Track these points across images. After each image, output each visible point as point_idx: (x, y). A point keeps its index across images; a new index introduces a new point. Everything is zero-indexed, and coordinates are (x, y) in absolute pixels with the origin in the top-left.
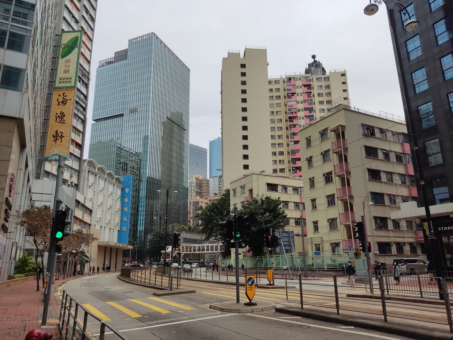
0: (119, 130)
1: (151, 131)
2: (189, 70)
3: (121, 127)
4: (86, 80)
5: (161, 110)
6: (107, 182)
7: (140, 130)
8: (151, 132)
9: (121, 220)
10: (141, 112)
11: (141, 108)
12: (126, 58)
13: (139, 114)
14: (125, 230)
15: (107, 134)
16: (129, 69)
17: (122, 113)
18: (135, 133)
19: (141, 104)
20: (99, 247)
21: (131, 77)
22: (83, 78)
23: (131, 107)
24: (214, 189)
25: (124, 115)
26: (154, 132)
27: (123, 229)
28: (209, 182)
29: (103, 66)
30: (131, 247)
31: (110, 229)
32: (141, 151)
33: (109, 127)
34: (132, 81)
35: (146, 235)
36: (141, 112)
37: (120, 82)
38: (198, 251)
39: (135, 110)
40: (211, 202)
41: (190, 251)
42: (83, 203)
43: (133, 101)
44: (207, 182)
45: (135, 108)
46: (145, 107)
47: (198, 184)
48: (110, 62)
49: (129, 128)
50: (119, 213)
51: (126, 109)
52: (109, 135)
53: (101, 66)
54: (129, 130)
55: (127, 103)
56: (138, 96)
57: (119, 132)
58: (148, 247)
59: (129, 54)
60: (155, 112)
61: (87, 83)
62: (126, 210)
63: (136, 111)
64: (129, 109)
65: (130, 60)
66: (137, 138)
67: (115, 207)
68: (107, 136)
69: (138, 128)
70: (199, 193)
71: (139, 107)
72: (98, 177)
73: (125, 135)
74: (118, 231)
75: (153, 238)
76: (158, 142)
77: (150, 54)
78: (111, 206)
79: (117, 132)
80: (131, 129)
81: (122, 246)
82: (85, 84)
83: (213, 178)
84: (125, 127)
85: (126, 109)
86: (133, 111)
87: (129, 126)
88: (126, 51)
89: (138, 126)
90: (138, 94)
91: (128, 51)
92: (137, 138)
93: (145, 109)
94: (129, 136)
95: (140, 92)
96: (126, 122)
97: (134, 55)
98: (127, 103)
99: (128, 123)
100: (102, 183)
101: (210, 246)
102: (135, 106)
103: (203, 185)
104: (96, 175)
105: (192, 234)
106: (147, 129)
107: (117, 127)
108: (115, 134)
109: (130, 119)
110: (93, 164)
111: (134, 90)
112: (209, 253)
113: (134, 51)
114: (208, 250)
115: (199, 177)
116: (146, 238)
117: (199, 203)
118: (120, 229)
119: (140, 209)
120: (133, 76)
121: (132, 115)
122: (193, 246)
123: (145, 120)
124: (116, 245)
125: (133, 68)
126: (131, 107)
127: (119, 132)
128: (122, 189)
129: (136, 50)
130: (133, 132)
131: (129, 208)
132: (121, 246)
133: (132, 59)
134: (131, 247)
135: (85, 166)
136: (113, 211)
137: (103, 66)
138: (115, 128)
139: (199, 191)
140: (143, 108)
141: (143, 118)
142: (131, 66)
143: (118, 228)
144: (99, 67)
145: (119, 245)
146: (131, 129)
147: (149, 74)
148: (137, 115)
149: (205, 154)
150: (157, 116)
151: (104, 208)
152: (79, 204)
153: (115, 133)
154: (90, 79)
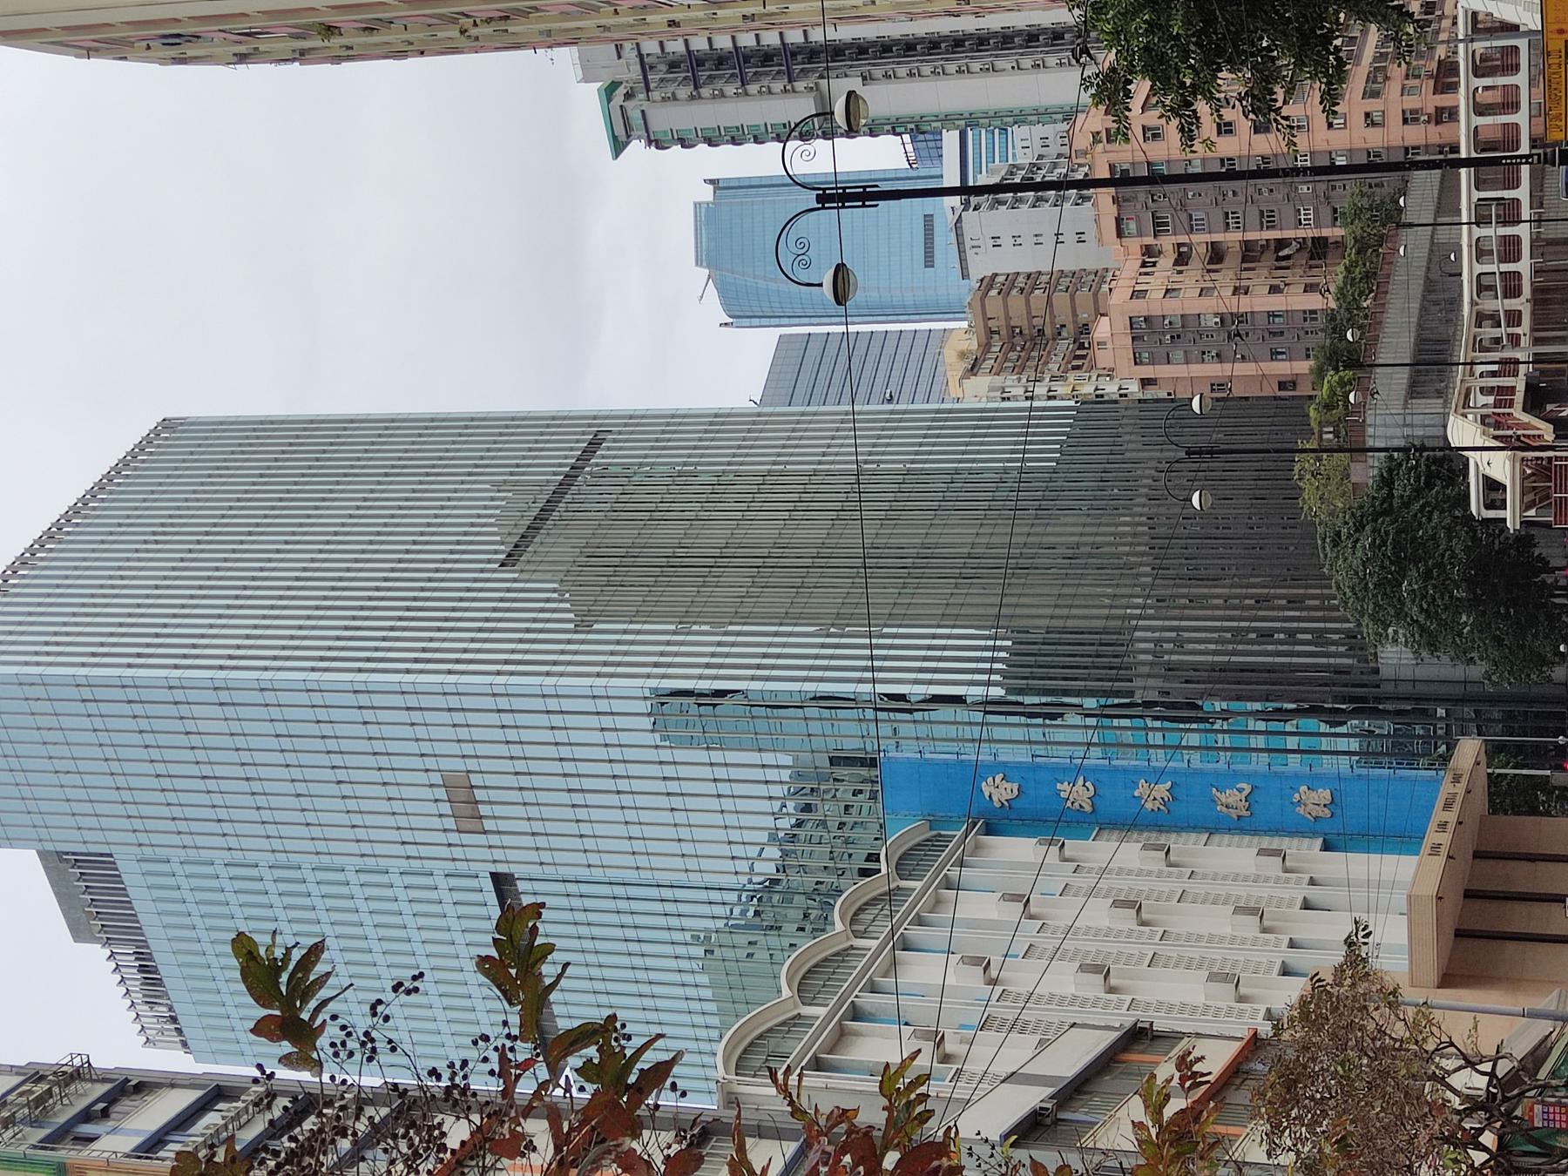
0: (610, 904)
1: (598, 675)
2: (168, 424)
3: (585, 888)
4: (85, 1095)
5: (454, 609)
6: (916, 933)
7: (601, 753)
8: (612, 675)
9: (1240, 826)
10: (468, 749)
11: (440, 748)
12: (105, 862)
13: (486, 765)
14: (1324, 795)
15: (645, 989)
16: (175, 839)
17: (488, 885)
18: (623, 785)
19: (413, 747)
20: (1448, 980)
21: (227, 828)
22: (62, 1119)
23: (436, 823)
25: (501, 868)
26: (612, 653)
28: (1001, 279)
29: (174, 1020)
30: (1469, 750)
31: (1307, 906)
33: (595, 972)
34: (254, 816)
36: (468, 749)
37: (375, 945)
38: (1516, 258)
39: (462, 794)
40: (1133, 226)
41: (1514, 318)
42: (1050, 1091)
43: (397, 806)
44: (994, 292)
45: (441, 793)
46: (430, 717)
47: (1014, 356)
48: (142, 969)
49: (585, 829)
50: (1186, 845)
51: (458, 852)
52: (653, 976)
53: (179, 1031)
54: (600, 829)
55: (412, 851)
56: (355, 775)
57: (623, 905)
58: (1477, 671)
59: (71, 842)
60: (465, 651)
61: (102, 1089)
62: (1162, 790)
64: (454, 838)
65: (112, 836)
66: (656, 770)
67: (1130, 872)
68: (657, 990)
69: (584, 768)
70: (1081, 347)
71: (430, 763)
72: (868, 1001)
73: (642, 861)
74: (1327, 847)
75: (1400, 615)
77: (55, 692)
79: (627, 919)
80: (596, 814)
81: (1457, 807)
82: (112, 1098)
83: (970, 253)
84: (580, 858)
85: (458, 852)
86: (466, 809)
87: (573, 828)
88: (58, 864)
89: (569, 767)
90: (341, 774)
91: (49, 847)
92: (656, 770)
93: (445, 717)
94: (649, 831)
95: (324, 760)
96: (546, 856)
97: (77, 808)
98: (412, 851)
99: (556, 842)
100: (921, 971)
101: (1476, 195)
102: (427, 793)
104: (856, 1014)
105: (1376, 338)
106: (588, 705)
107: (592, 917)
108: (643, 934)
109: (524, 826)
110: (760, 1037)
111: (320, 803)
112: (1537, 200)
113: (44, 806)
114: (1510, 250)
115: (963, 355)
117: (1146, 319)
118: (1313, 834)
120: (222, 813)
121: (499, 810)
122: (1473, 303)
123: (522, 719)
124: (1444, 851)
125: (165, 811)
126: (436, 823)
127: (623, 905)
128: (990, 830)
129: (39, 792)
130: (613, 800)
131: (1138, 772)
133: (105, 823)
134: (1469, 750)
136: (1164, 886)
137: (174, 1020)
138: (596, 931)
139: (1064, 346)
140: (436, 733)
141: (512, 735)
142: (150, 824)
143: (1307, 851)
144: (184, 1044)
145: (1436, 848)
146: (596, 814)
147: (193, 695)
148: (491, 780)
149: (814, 349)
151: (1134, 949)
152: (1057, 1121)
153: (631, 933)
154: (77, 1062)
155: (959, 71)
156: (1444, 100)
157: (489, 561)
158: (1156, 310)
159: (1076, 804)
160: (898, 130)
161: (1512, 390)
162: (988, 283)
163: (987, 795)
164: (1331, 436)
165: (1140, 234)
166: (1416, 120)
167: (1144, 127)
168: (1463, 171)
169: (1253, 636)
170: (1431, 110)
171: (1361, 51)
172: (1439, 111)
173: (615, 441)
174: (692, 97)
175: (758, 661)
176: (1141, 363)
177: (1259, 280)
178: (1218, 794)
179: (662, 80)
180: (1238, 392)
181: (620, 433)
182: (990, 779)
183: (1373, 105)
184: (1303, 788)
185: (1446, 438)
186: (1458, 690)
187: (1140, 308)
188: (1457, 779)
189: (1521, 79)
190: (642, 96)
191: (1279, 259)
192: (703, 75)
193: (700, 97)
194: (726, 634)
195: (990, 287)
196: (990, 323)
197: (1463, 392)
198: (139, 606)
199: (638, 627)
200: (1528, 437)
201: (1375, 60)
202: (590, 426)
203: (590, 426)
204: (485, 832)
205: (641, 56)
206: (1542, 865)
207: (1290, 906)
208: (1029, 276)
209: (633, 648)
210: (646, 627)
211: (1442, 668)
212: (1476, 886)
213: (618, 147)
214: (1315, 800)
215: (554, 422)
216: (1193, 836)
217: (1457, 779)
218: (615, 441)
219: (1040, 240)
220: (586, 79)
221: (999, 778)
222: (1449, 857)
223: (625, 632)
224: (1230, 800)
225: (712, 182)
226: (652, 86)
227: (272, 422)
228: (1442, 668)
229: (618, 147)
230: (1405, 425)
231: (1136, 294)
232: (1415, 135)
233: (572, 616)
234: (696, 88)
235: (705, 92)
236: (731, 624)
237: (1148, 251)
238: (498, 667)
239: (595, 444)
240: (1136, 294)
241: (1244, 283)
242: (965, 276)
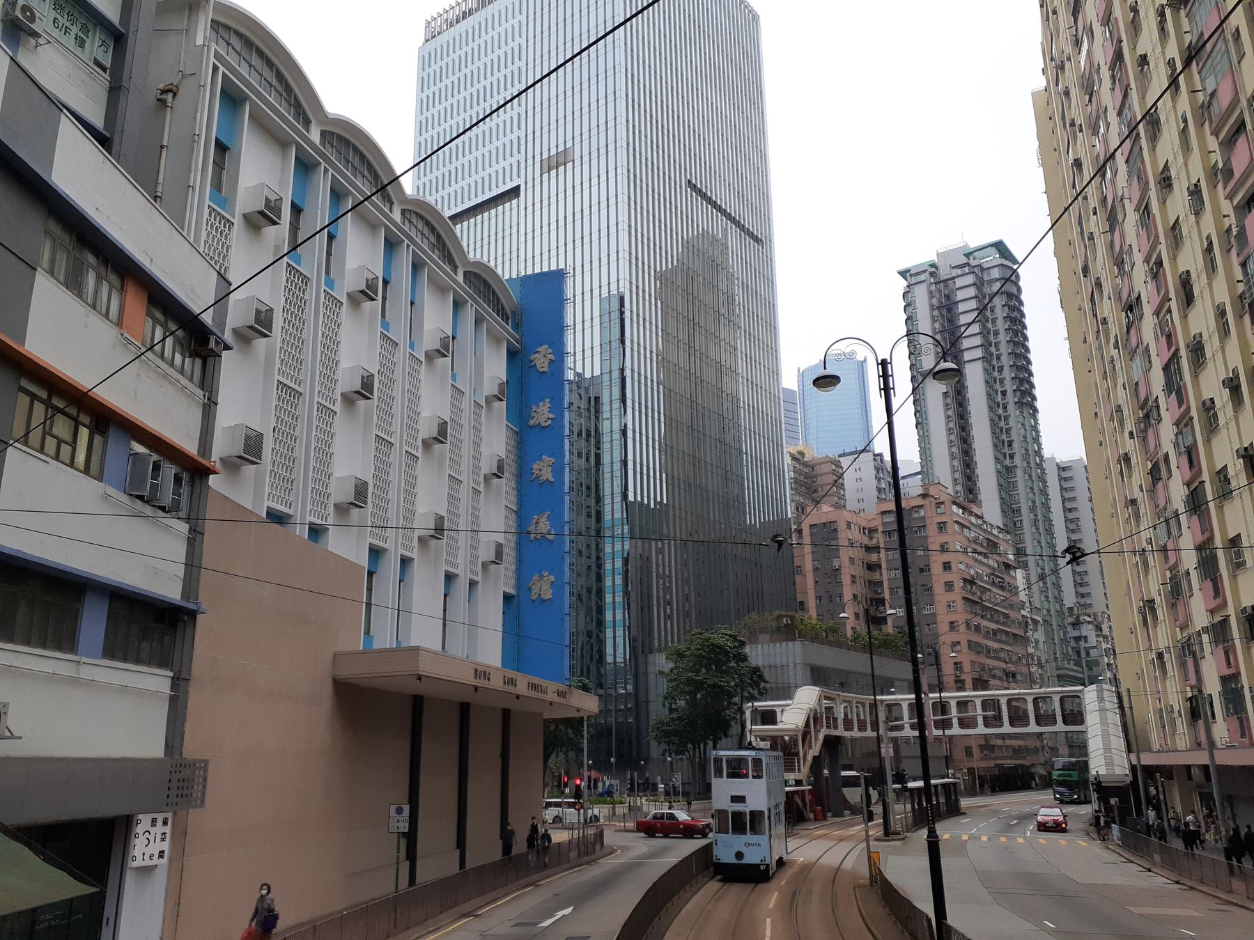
2: (755, 18)
9: (522, 533)
14: (548, 595)
24: (860, 496)
27: (535, 590)
31: (450, 578)
32: (597, 373)
35: (641, 658)
39: (561, 160)
44: (834, 467)
48: (464, 13)
50: (505, 485)
60: (641, 180)
62: (547, 474)
63: (567, 160)
74: (508, 598)
76: (640, 404)
78: (440, 519)
81: (533, 694)
86: (554, 163)
103: (818, 483)
116: (641, 669)
117: (835, 529)
118: (519, 586)
119: (608, 549)
124: (481, 683)
128: (512, 354)
132: (522, 688)
135: (199, 42)
143: (503, 580)
144: (427, 41)
145: (512, 682)
150: (645, 220)
155: (951, 441)
156: (969, 683)
157: (691, 174)
158: (840, 534)
159: (534, 414)
160: (918, 414)
161: (836, 727)
162: (838, 465)
163: (539, 349)
164: (785, 622)
165: (884, 524)
166: (957, 669)
167: (945, 522)
168: (914, 696)
169: (668, 597)
170: (963, 677)
171: (989, 639)
172: (963, 681)
173: (758, 250)
174: (932, 306)
175: (642, 344)
176: (811, 529)
177: (860, 589)
178: (546, 516)
179: (940, 291)
180: (798, 578)
181: (762, 253)
182: (550, 350)
183: (964, 645)
184: (552, 578)
185: (797, 687)
186: (642, 697)
187: (842, 526)
188: (561, 694)
189: (1033, 727)
190: (932, 280)
191: (871, 600)
192: (944, 312)
193: (933, 310)
194: (656, 299)
195: (836, 466)
196: (818, 467)
197: (833, 696)
198: (656, 96)
199: (660, 334)
200: (810, 740)
201: (987, 647)
202: (766, 237)
203: (766, 237)
204: (541, 175)
205: (953, 278)
206: (498, 763)
207: (448, 562)
208: (842, 485)
209: (647, 303)
210: (662, 395)
211: (658, 688)
212: (509, 714)
213: (903, 274)
214: (543, 587)
215: (766, 219)
216: (514, 500)
217: (561, 694)
218: (758, 250)
219: (860, 491)
220: (938, 254)
221: (551, 357)
222: (476, 689)
223: (657, 326)
224: (542, 525)
225: (865, 360)
226: (938, 286)
227: (760, 71)
228: (658, 688)
229: (903, 274)
230: (795, 664)
231: (849, 524)
232: (948, 668)
233: (664, 269)
234: (938, 308)
235: (936, 313)
236: (662, 302)
237: (872, 531)
238: (632, 198)
239: (756, 239)
240: (849, 524)
241: (858, 582)
242: (840, 456)
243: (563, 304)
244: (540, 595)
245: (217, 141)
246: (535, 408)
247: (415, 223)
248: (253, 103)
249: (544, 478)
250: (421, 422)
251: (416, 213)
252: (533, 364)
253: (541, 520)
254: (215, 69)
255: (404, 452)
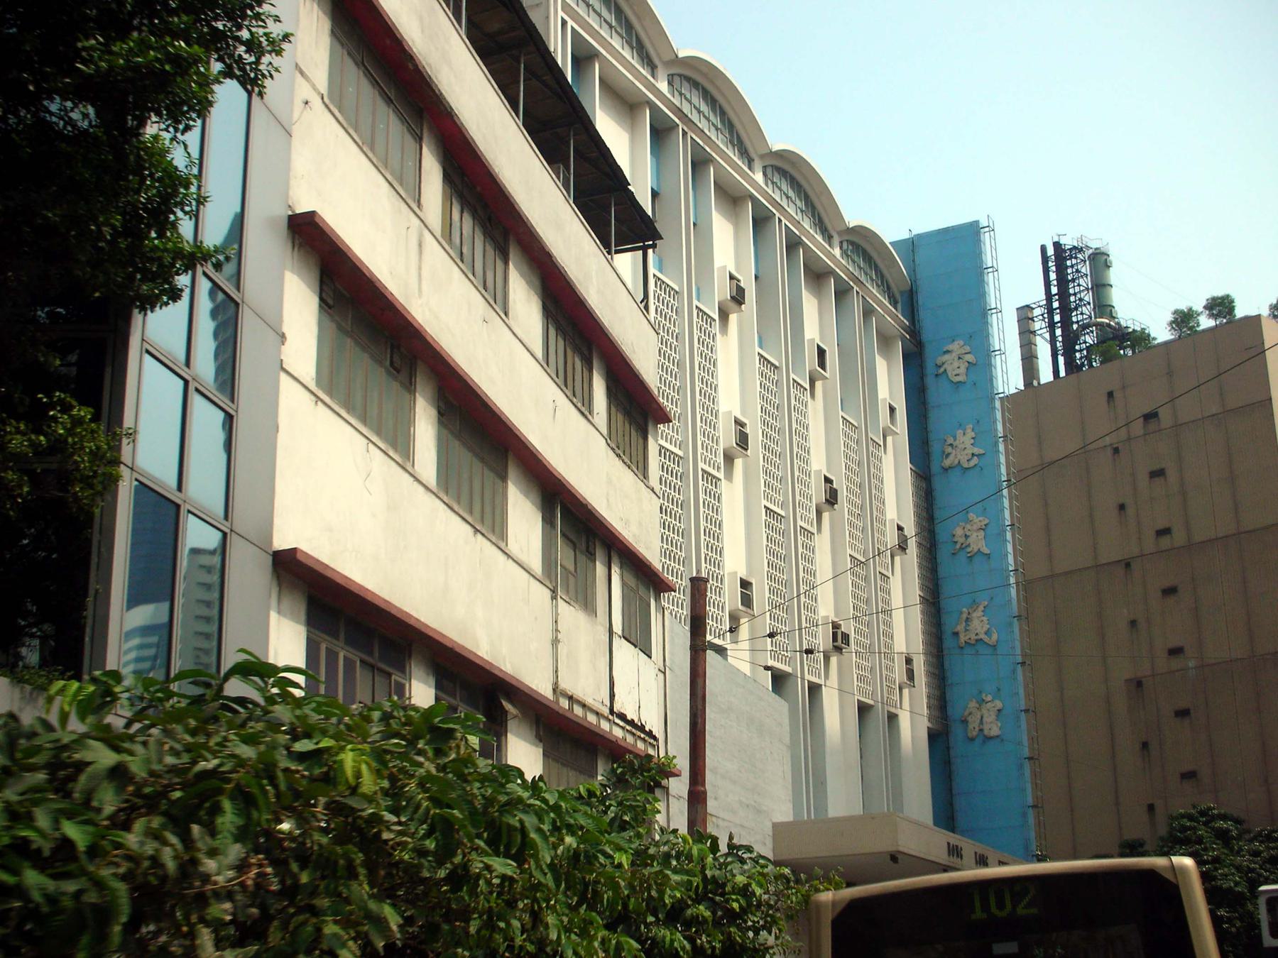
27: (974, 724)
159: (949, 450)
243: (982, 274)
244: (981, 730)
245: (652, 189)
246: (950, 440)
247: (688, 96)
248: (605, 64)
249: (974, 548)
250: (721, 425)
251: (688, 79)
252: (942, 370)
253: (975, 615)
254: (564, 23)
255: (799, 528)
